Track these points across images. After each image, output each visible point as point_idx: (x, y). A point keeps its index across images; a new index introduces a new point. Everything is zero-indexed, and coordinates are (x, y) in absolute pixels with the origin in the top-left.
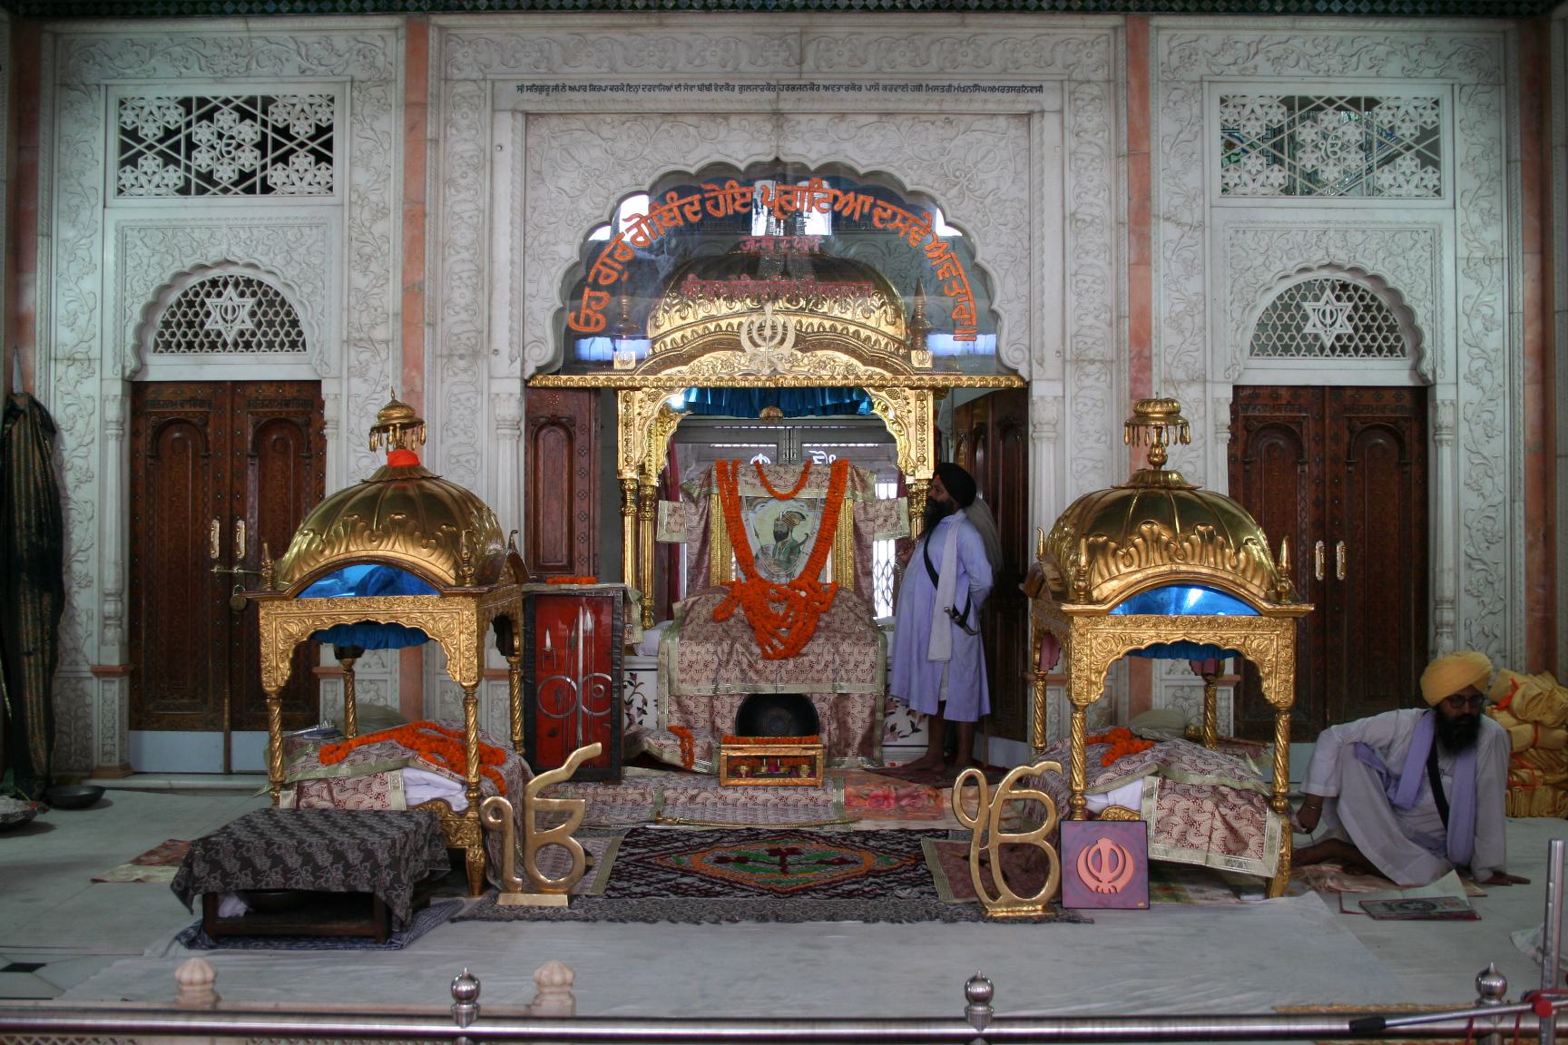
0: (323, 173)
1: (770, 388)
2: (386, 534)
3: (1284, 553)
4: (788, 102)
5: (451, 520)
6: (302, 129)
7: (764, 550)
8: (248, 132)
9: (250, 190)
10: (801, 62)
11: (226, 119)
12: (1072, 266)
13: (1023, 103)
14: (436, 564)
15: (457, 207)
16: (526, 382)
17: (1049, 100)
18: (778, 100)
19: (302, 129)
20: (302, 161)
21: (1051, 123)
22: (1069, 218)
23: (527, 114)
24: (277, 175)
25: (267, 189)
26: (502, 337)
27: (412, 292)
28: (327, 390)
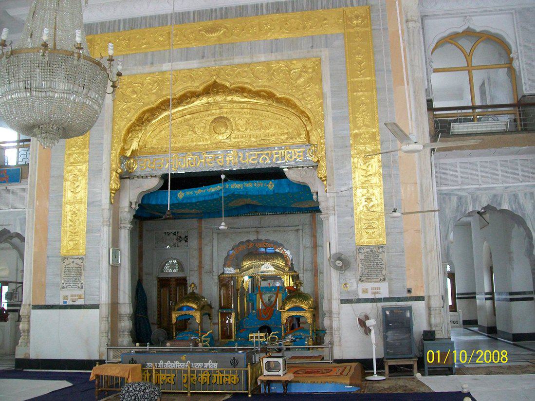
0: (186, 243)
1: (386, 394)
2: (188, 302)
3: (500, 339)
4: (259, 229)
5: (198, 300)
6: (183, 237)
7: (367, 157)
8: (175, 237)
9: (175, 247)
10: (260, 223)
11: (171, 235)
12: (305, 255)
13: (297, 228)
14: (195, 306)
15: (207, 250)
16: (219, 276)
17: (300, 227)
18: (232, 98)
19: (183, 237)
20: (183, 242)
21: (301, 231)
22: (304, 247)
23: (218, 233)
24: (179, 244)
25: (178, 246)
26: (214, 269)
27: (200, 262)
28: (188, 278)
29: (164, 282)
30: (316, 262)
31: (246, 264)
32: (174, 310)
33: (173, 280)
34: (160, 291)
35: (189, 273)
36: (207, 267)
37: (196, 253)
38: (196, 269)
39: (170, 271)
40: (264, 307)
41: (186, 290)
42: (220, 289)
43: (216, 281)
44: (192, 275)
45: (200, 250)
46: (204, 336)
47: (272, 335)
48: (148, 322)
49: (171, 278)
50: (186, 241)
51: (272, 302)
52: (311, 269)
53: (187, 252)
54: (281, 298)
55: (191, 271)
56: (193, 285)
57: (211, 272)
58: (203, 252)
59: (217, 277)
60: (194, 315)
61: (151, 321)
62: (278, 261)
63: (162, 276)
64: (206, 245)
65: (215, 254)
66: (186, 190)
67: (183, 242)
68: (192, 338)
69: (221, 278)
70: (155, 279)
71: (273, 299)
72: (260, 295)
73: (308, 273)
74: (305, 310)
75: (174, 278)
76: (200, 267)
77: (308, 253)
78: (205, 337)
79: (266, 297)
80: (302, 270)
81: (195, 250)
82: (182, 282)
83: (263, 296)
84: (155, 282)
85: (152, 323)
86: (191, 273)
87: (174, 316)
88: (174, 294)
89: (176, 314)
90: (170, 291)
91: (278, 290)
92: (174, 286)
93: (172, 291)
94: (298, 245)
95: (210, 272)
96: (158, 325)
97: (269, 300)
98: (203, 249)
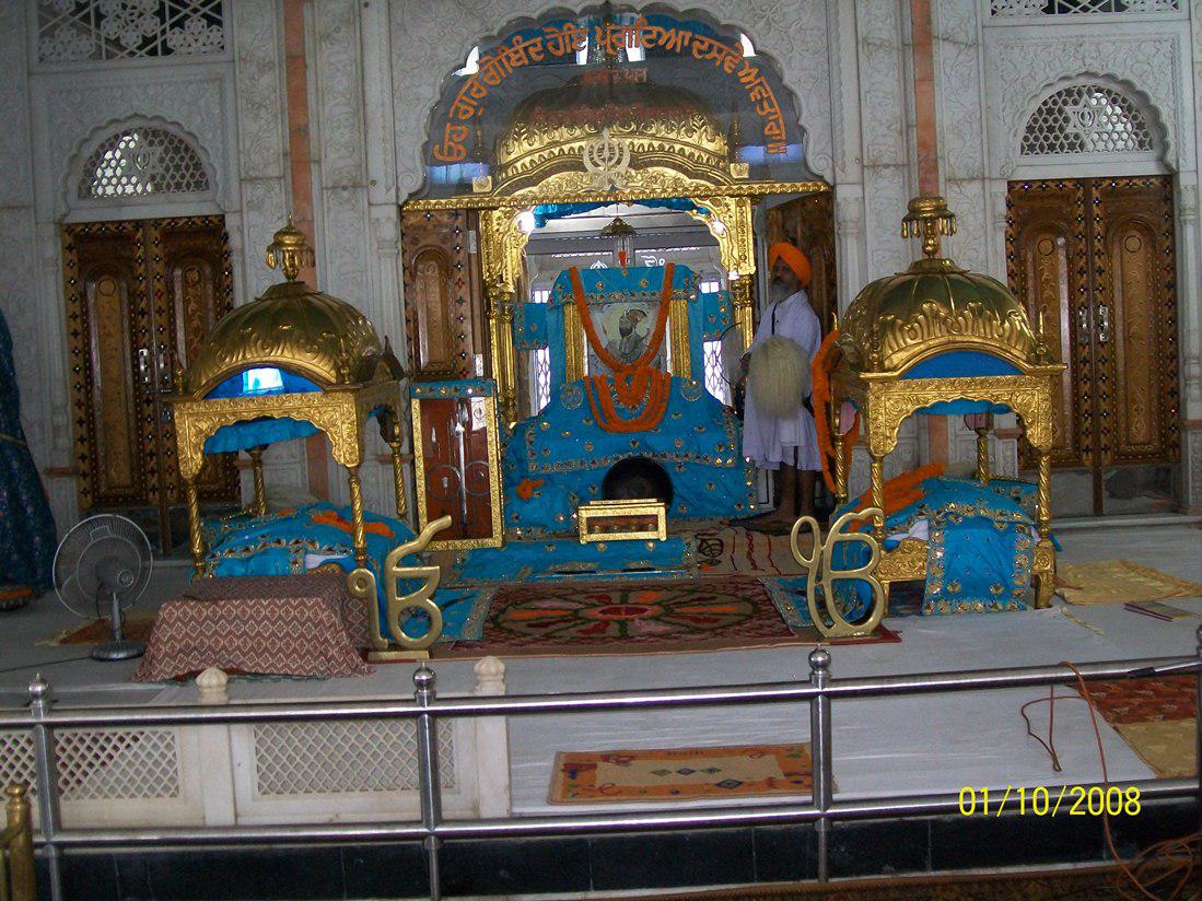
5: (331, 329)
9: (153, 52)
15: (329, 67)
20: (196, 24)
24: (175, 38)
25: (167, 51)
26: (378, 167)
28: (231, 222)
29: (99, 250)
30: (928, 125)
31: (523, 151)
32: (188, 393)
33: (155, 234)
34: (84, 296)
35: (235, 196)
36: (333, 156)
37: (270, 84)
38: (273, 171)
39: (129, 189)
40: (603, 370)
41: (223, 287)
42: (410, 273)
43: (390, 231)
44: (257, 206)
45: (295, 64)
46: (400, 551)
47: (843, 530)
48: (28, 464)
49: (138, 224)
50: (211, 21)
51: (639, 340)
52: (902, 158)
53: (220, 80)
54: (682, 322)
55: (253, 180)
56: (288, 240)
57: (358, 183)
58: (310, 75)
59: (393, 212)
60: (320, 419)
61: (42, 456)
62: (690, 131)
63: (85, 214)
64: (327, 37)
65: (376, 90)
66: (22, 815)
67: (196, 24)
68: (314, 561)
69: (413, 220)
70: (51, 230)
71: (644, 328)
72: (580, 309)
73: (883, 183)
74: (1018, 371)
75: (157, 222)
76: (299, 158)
77: (885, 79)
78: (406, 560)
79: (608, 322)
80: (853, 171)
81: (264, 67)
82: (202, 245)
83: (597, 318)
84: (53, 249)
85: (51, 472)
86: (250, 192)
87: (193, 430)
88: (160, 311)
89: (198, 416)
90: (134, 296)
91: (670, 285)
92: (159, 268)
93: (142, 295)
94: (830, 34)
95: (355, 186)
96: (84, 475)
97: (624, 332)
98: (309, 61)
